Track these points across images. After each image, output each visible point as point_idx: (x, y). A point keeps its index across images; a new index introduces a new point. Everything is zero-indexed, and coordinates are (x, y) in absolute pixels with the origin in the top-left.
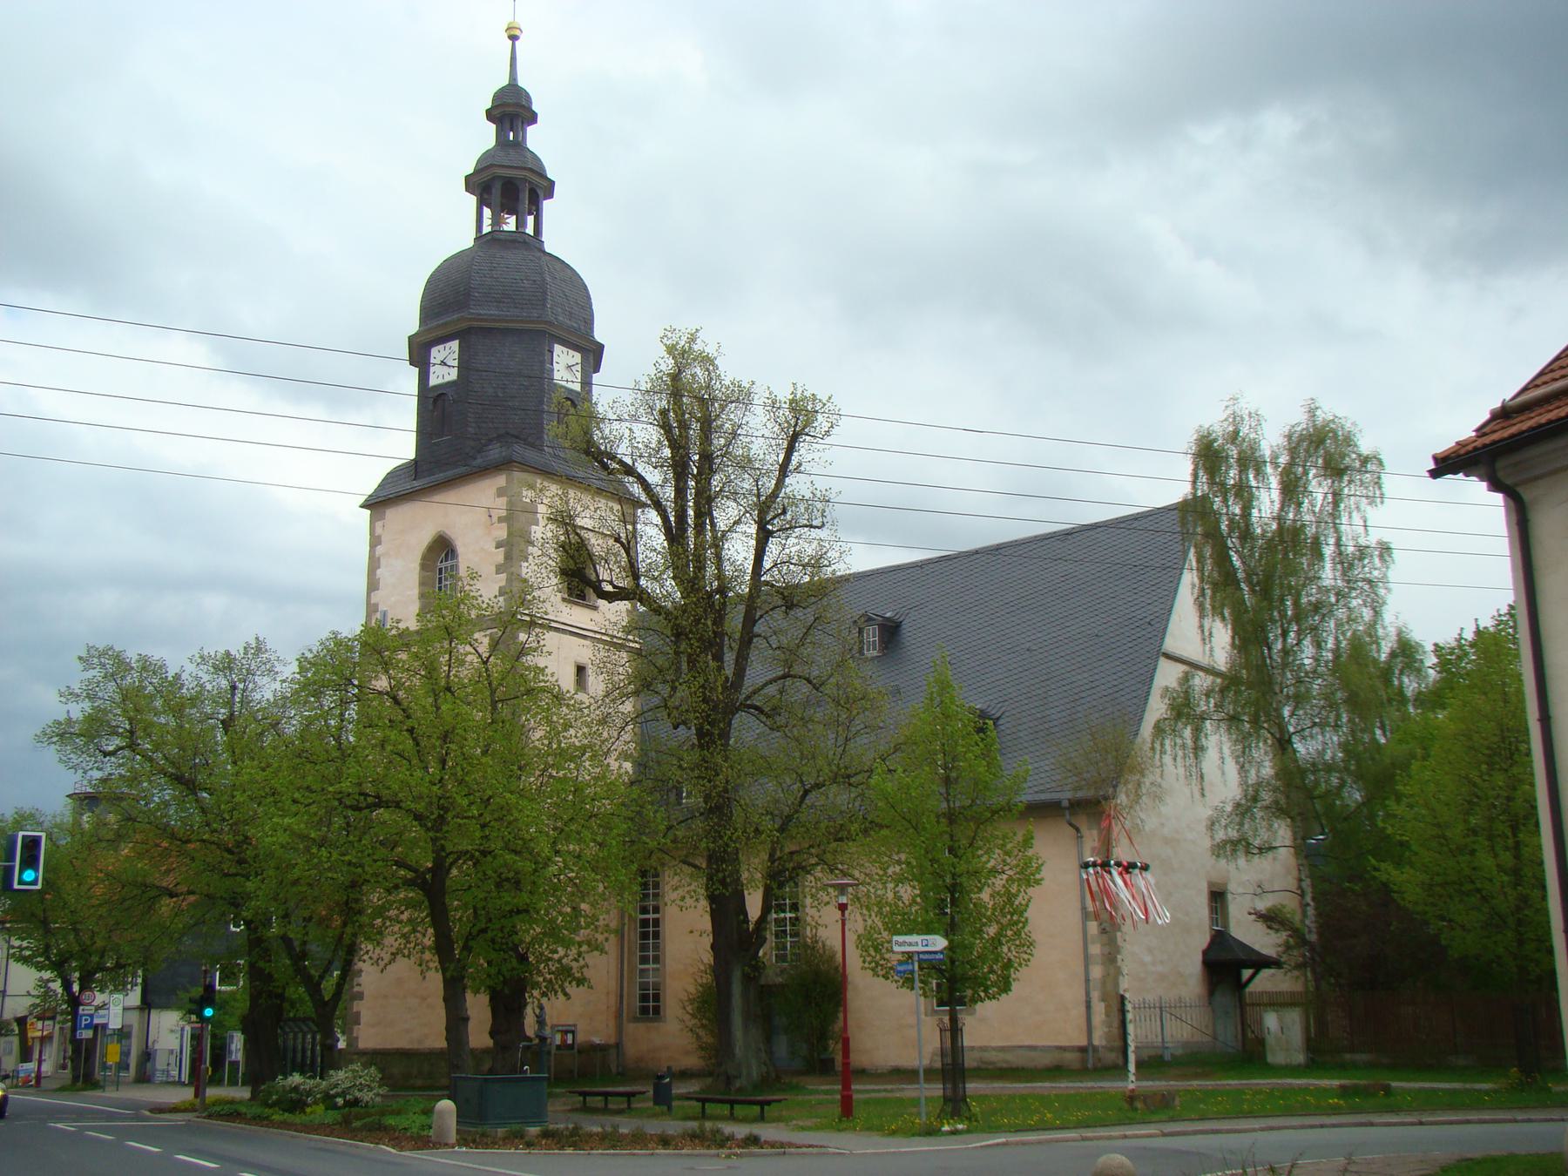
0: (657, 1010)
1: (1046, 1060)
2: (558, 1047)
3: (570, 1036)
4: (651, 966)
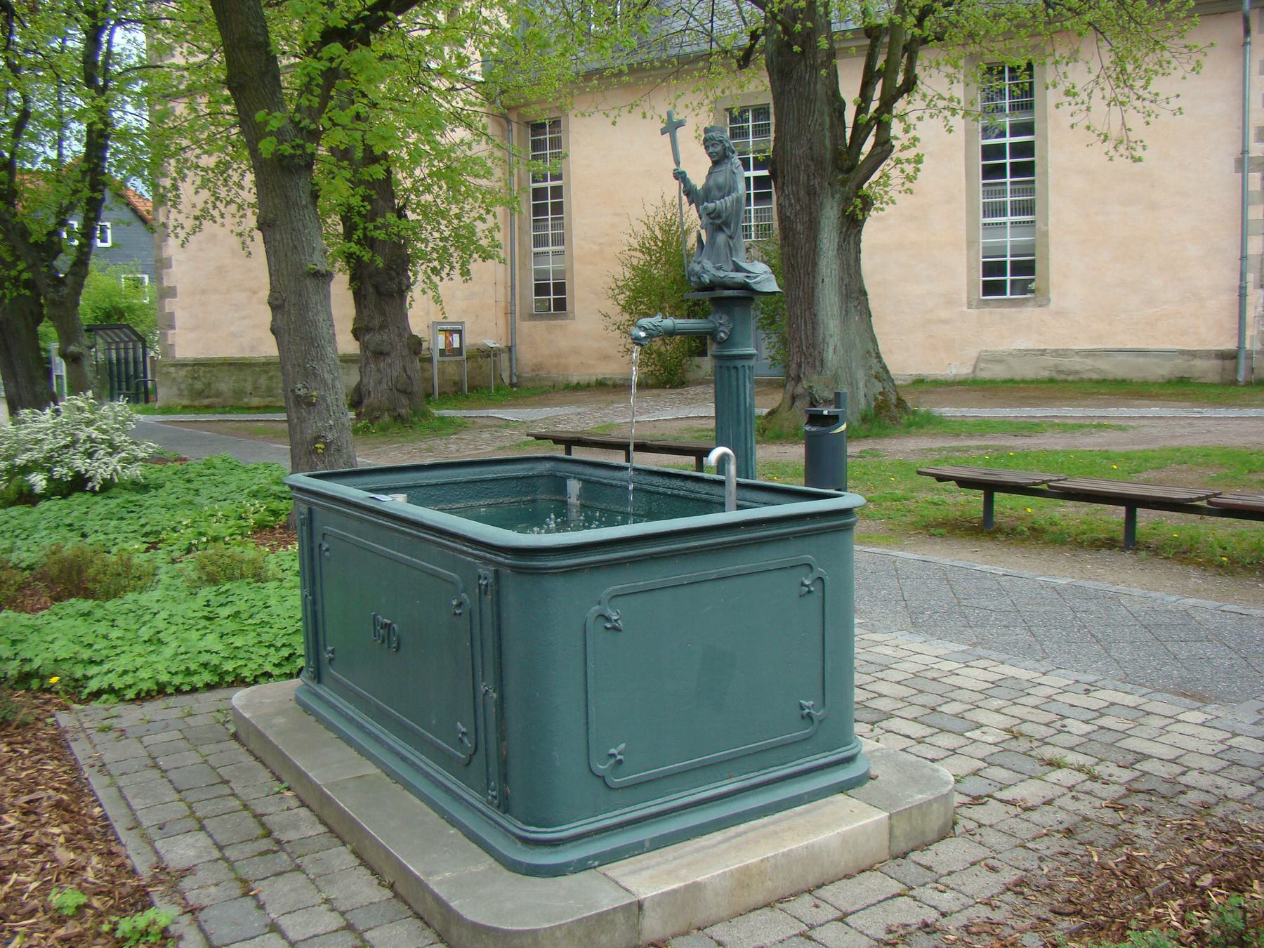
0: (561, 305)
1: (1163, 370)
2: (442, 352)
3: (456, 337)
4: (550, 248)
